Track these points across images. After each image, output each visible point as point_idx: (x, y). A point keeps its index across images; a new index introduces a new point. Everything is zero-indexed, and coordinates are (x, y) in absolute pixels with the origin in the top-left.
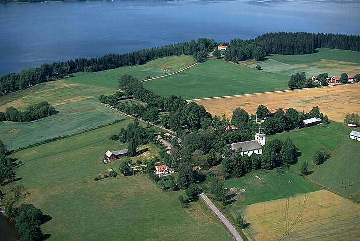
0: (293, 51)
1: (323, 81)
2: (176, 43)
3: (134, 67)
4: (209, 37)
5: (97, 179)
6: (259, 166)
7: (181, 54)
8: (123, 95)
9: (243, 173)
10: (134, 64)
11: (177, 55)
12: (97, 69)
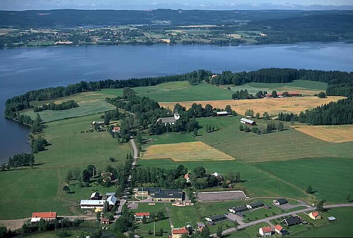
0: (270, 80)
1: (260, 95)
2: (180, 74)
3: (148, 87)
4: (206, 68)
5: (82, 132)
6: (170, 130)
7: (183, 80)
8: (121, 98)
9: (160, 133)
10: (147, 85)
11: (181, 80)
12: (119, 87)
